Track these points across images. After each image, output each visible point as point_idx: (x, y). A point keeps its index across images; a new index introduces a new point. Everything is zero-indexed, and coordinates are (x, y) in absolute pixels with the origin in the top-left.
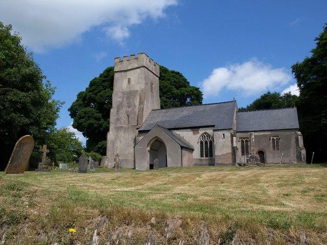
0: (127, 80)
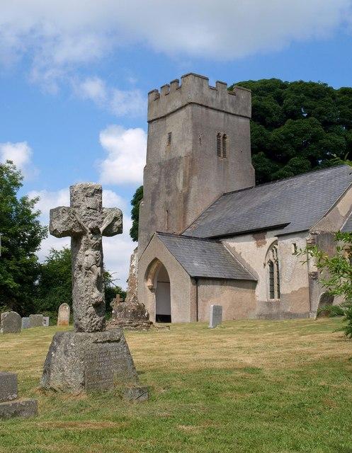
0: (166, 137)
